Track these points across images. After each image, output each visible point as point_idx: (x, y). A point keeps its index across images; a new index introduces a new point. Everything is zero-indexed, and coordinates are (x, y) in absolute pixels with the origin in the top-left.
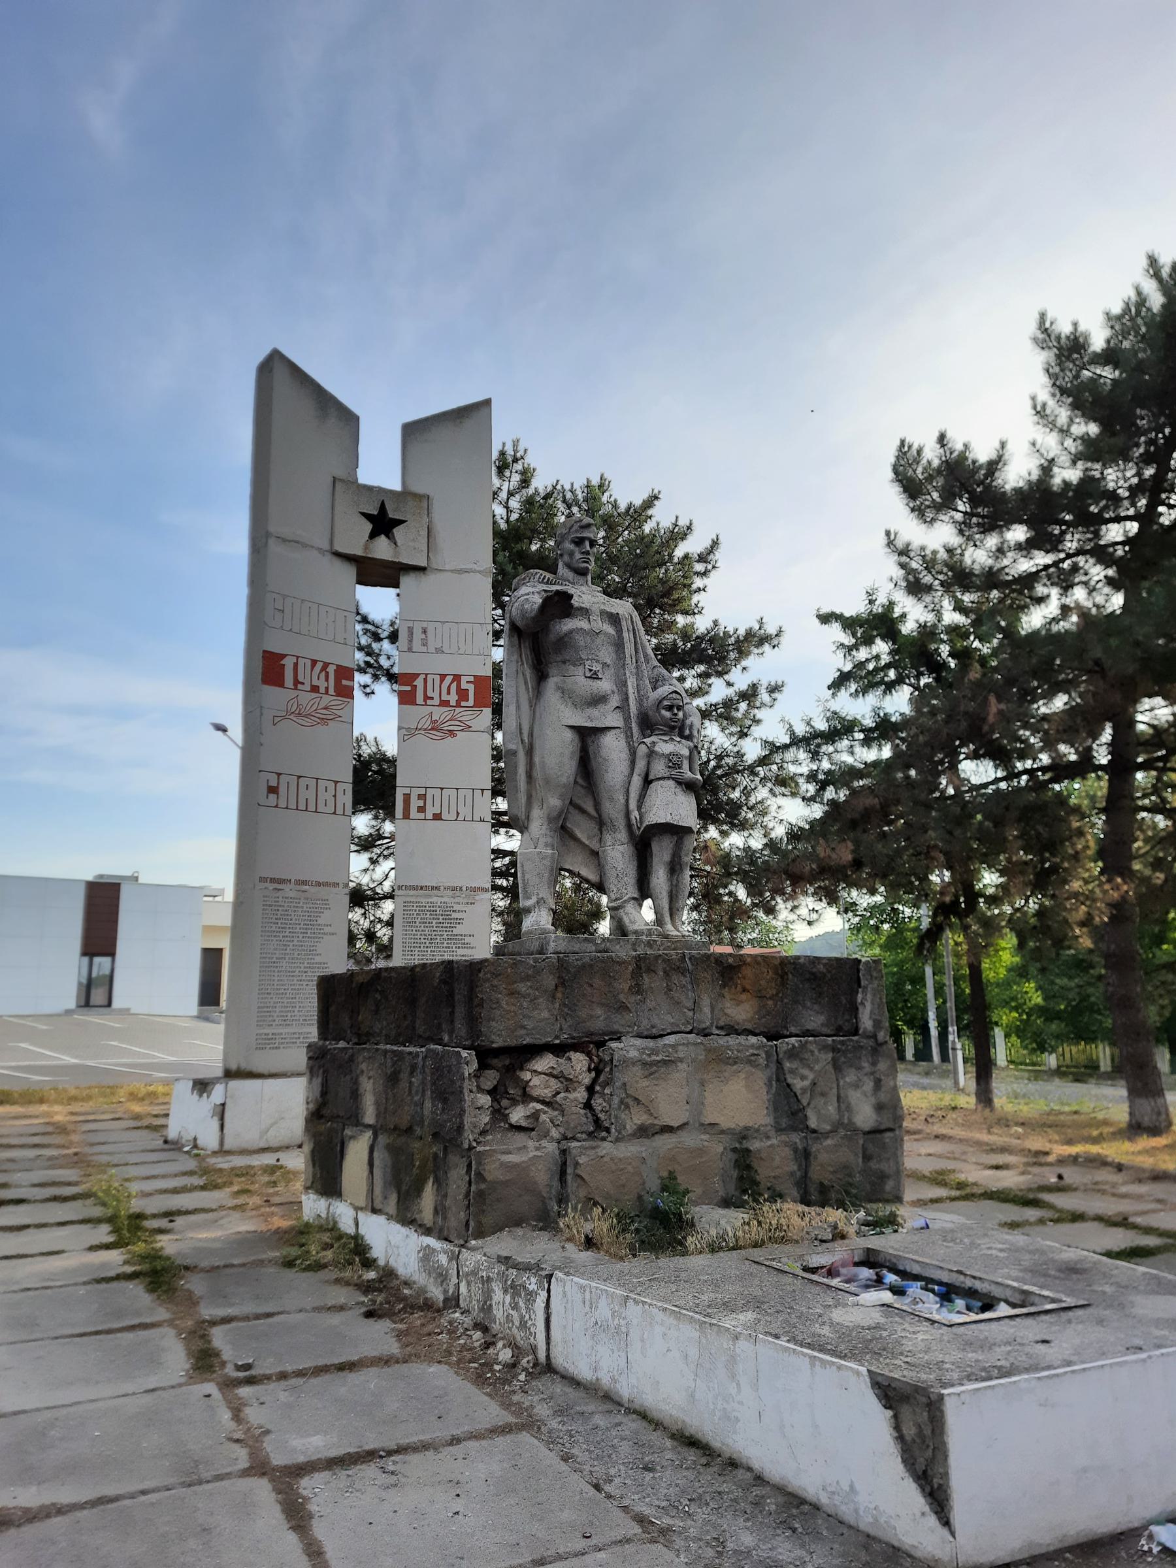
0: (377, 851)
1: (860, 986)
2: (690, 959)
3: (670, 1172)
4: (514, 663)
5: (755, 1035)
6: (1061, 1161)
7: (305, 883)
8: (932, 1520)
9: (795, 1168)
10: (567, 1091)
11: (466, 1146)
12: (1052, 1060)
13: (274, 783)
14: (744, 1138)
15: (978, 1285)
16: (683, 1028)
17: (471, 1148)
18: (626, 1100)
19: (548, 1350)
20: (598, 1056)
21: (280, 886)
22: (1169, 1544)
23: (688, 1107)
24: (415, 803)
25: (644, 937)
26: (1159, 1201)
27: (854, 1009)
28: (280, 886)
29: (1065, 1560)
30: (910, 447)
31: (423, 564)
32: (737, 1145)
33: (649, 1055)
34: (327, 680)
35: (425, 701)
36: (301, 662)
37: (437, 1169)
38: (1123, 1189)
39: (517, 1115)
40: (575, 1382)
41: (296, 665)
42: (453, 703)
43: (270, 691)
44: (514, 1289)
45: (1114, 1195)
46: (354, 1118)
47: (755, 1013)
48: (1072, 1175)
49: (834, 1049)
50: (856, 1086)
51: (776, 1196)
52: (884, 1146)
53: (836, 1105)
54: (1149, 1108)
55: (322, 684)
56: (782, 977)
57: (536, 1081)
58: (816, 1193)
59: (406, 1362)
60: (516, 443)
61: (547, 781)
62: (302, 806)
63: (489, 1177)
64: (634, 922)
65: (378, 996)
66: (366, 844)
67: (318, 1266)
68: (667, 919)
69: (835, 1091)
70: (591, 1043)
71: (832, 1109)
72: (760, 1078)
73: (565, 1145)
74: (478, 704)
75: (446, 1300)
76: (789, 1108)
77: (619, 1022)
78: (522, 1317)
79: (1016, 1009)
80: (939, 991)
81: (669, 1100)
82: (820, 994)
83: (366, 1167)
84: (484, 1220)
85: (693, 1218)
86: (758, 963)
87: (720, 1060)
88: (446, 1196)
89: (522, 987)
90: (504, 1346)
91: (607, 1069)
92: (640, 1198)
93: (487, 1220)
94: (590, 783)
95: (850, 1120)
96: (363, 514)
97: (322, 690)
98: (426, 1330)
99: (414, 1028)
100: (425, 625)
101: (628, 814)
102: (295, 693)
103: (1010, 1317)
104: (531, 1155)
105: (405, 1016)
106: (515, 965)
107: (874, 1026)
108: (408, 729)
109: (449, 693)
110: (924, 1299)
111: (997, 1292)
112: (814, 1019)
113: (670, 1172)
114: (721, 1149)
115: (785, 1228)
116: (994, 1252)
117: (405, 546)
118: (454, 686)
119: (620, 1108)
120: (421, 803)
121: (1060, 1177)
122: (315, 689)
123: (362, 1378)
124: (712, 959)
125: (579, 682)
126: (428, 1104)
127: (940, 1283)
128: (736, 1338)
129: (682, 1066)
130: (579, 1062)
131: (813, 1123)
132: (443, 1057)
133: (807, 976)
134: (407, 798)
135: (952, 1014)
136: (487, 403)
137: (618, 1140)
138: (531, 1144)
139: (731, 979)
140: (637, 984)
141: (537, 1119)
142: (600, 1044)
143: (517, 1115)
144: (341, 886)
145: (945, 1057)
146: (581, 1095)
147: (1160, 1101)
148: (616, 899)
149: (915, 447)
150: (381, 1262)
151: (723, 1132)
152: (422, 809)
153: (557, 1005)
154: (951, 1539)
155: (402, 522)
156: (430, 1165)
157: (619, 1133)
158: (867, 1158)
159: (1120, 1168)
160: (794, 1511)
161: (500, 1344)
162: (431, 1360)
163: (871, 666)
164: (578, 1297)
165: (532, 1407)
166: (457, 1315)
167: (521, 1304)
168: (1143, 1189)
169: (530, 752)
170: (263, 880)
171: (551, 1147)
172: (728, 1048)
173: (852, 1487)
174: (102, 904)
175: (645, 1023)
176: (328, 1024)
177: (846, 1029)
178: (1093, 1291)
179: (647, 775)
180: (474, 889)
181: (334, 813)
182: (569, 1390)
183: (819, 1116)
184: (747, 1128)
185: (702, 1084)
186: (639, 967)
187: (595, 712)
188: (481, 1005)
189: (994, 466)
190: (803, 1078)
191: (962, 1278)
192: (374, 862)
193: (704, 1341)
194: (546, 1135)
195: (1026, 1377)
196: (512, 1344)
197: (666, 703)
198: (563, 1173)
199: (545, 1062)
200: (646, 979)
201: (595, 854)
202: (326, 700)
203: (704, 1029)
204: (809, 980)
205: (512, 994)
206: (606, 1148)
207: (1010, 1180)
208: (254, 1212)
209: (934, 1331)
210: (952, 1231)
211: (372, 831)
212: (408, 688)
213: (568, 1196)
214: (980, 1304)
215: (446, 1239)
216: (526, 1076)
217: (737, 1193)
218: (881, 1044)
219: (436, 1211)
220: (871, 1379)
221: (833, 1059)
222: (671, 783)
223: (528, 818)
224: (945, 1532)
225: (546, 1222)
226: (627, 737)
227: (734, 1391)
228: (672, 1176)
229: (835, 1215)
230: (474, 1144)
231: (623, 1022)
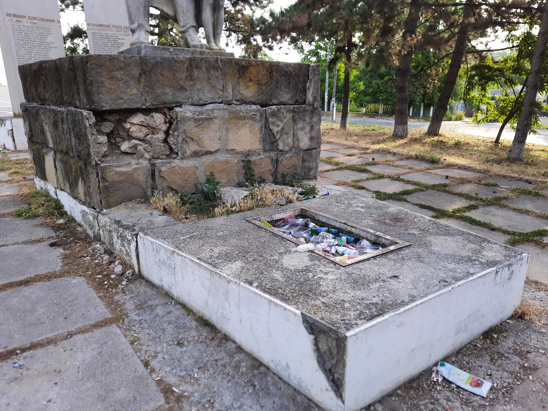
1: (308, 79)
2: (221, 61)
3: (211, 173)
5: (255, 104)
6: (373, 152)
7: (34, 18)
8: (332, 394)
9: (272, 168)
10: (153, 134)
11: (94, 163)
12: (364, 110)
14: (248, 155)
15: (353, 230)
16: (217, 100)
17: (97, 164)
18: (186, 139)
19: (139, 268)
20: (170, 115)
22: (447, 377)
23: (220, 142)
25: (198, 49)
26: (410, 168)
27: (304, 91)
29: (398, 395)
32: (245, 159)
33: (198, 115)
37: (83, 174)
38: (397, 163)
39: (125, 146)
40: (152, 285)
44: (122, 237)
45: (393, 166)
46: (45, 144)
47: (255, 93)
48: (378, 158)
49: (294, 112)
50: (302, 129)
51: (262, 181)
52: (311, 156)
53: (292, 138)
54: (401, 129)
56: (270, 73)
57: (133, 129)
58: (280, 178)
59: (61, 277)
63: (109, 180)
64: (193, 40)
67: (35, 216)
68: (212, 39)
69: (292, 132)
70: (166, 109)
71: (290, 140)
72: (257, 126)
73: (154, 161)
75: (94, 236)
76: (270, 141)
77: (180, 97)
78: (127, 251)
79: (355, 91)
80: (330, 85)
81: (210, 138)
82: (289, 83)
83: (54, 169)
84: (110, 200)
85: (220, 195)
86: (258, 65)
87: (237, 117)
88: (90, 187)
90: (119, 263)
91: (175, 123)
92: (195, 185)
93: (112, 200)
95: (298, 145)
98: (79, 255)
103: (374, 257)
104: (133, 167)
105: (57, 90)
107: (313, 100)
110: (327, 236)
111: (363, 234)
112: (286, 97)
113: (211, 173)
114: (236, 161)
115: (264, 199)
116: (359, 209)
119: (182, 143)
121: (373, 159)
123: (31, 290)
124: (233, 62)
126: (73, 140)
127: (334, 227)
128: (229, 282)
130: (158, 119)
131: (281, 147)
132: (75, 114)
133: (283, 73)
135: (334, 93)
137: (182, 159)
138: (133, 162)
139: (244, 73)
141: (136, 149)
142: (171, 109)
143: (125, 146)
144: (56, 21)
145: (329, 109)
146: (161, 136)
147: (405, 126)
148: (184, 26)
150: (69, 213)
151: (237, 153)
153: (142, 86)
154: (342, 405)
156: (79, 172)
157: (183, 155)
158: (304, 161)
159: (394, 154)
160: (256, 372)
161: (117, 262)
162: (77, 274)
164: (151, 247)
165: (125, 303)
166: (98, 245)
167: (126, 245)
168: (403, 163)
171: (145, 163)
172: (241, 111)
173: (287, 365)
175: (196, 98)
177: (300, 101)
178: (408, 234)
182: (148, 290)
183: (285, 144)
184: (249, 151)
185: (227, 130)
188: (91, 84)
190: (278, 126)
191: (346, 226)
193: (212, 279)
194: (142, 156)
195: (392, 314)
196: (123, 263)
198: (153, 175)
199: (138, 119)
200: (196, 73)
203: (229, 101)
204: (284, 75)
205: (111, 78)
206: (176, 163)
207: (355, 161)
208: (16, 184)
209: (336, 271)
210: (340, 196)
213: (157, 186)
214: (353, 239)
215: (93, 208)
216: (128, 126)
217: (244, 180)
218: (315, 109)
219: (85, 194)
220: (303, 318)
221: (293, 116)
224: (339, 402)
225: (145, 199)
227: (227, 306)
228: (212, 174)
229: (288, 191)
230: (99, 162)
231: (182, 96)
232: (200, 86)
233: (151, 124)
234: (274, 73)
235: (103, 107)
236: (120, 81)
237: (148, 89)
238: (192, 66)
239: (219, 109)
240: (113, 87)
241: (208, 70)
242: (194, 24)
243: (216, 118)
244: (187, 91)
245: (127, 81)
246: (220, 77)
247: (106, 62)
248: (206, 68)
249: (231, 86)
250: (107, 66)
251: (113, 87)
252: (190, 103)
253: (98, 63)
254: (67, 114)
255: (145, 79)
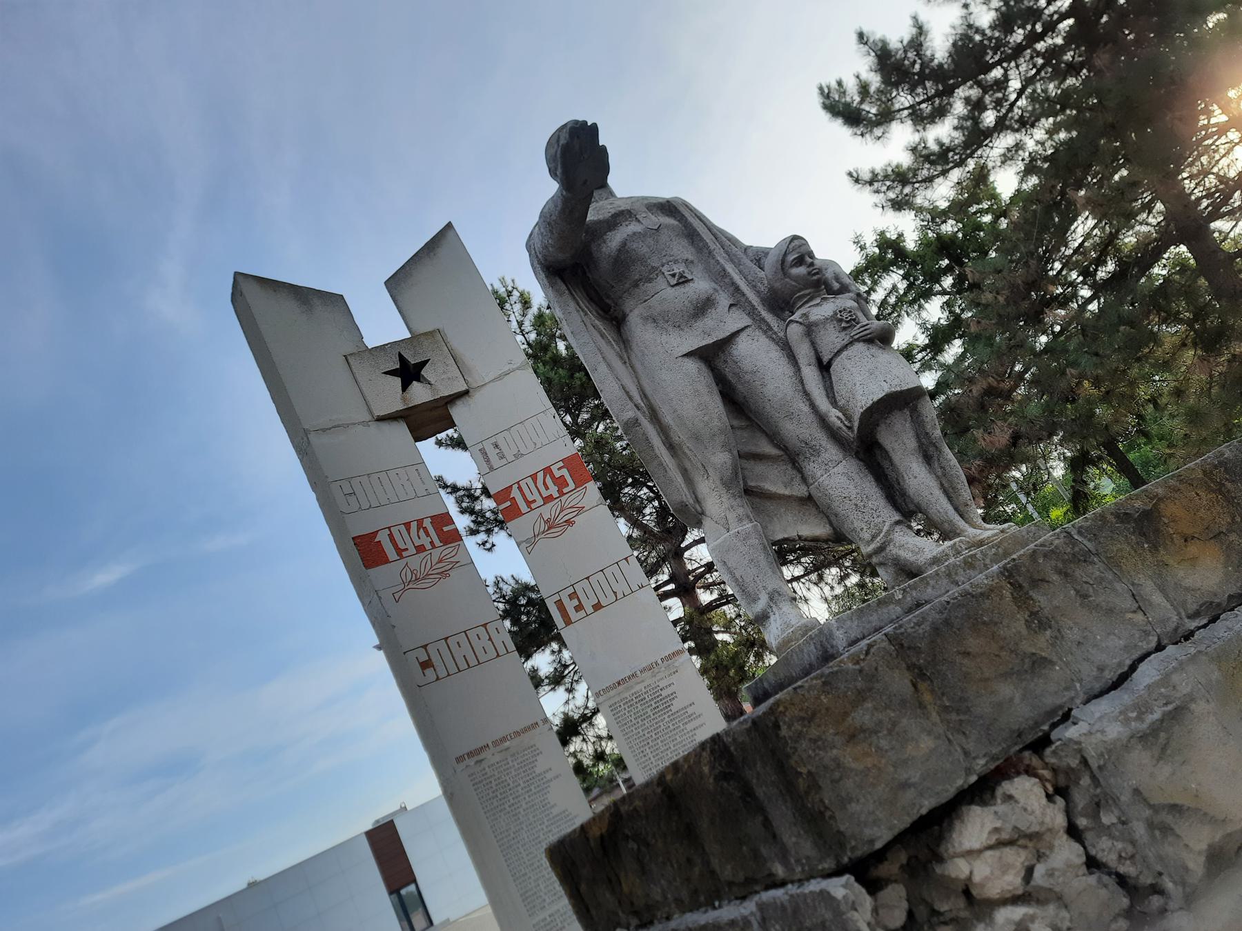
0: (568, 680)
2: (1080, 533)
4: (575, 314)
7: (504, 739)
10: (1040, 856)
13: (424, 658)
21: (480, 757)
24: (570, 605)
25: (952, 560)
28: (480, 757)
30: (829, 87)
31: (463, 388)
33: (1139, 718)
34: (428, 534)
35: (529, 506)
36: (523, 484)
41: (391, 536)
42: (556, 495)
43: (378, 572)
55: (425, 541)
60: (502, 281)
61: (697, 438)
62: (463, 665)
65: (633, 845)
66: (557, 679)
74: (579, 483)
89: (863, 716)
94: (749, 418)
96: (386, 373)
97: (428, 546)
99: (713, 872)
100: (493, 440)
101: (823, 421)
102: (403, 562)
105: (689, 860)
106: (828, 683)
108: (527, 541)
109: (547, 488)
117: (439, 380)
118: (548, 479)
119: (1153, 837)
120: (576, 602)
122: (420, 549)
125: (666, 295)
129: (1199, 707)
130: (1027, 795)
132: (796, 911)
134: (559, 604)
136: (449, 226)
139: (1157, 531)
140: (1032, 614)
144: (540, 723)
148: (874, 537)
149: (834, 85)
152: (579, 608)
153: (935, 717)
155: (424, 363)
157: (1184, 884)
163: (892, 300)
169: (654, 417)
170: (460, 759)
174: (386, 843)
175: (1088, 671)
176: (588, 911)
179: (819, 360)
180: (669, 657)
181: (498, 655)
186: (1017, 587)
187: (708, 322)
188: (815, 786)
189: (916, 44)
192: (570, 691)
197: (791, 258)
199: (975, 828)
200: (1041, 599)
201: (809, 500)
202: (436, 554)
203: (1176, 629)
205: (852, 737)
211: (555, 665)
212: (508, 504)
222: (860, 347)
223: (697, 500)
226: (765, 332)
232: (1076, 630)
233: (1023, 826)
234: (1228, 485)
235: (872, 842)
236: (876, 732)
237: (954, 716)
238: (1020, 586)
239: (1181, 666)
240: (869, 762)
241: (1066, 575)
242: (897, 517)
243: (1191, 698)
244: (1052, 663)
245: (894, 724)
246: (1110, 576)
247: (818, 698)
248: (1059, 572)
249: (1150, 582)
250: (827, 709)
251: (869, 762)
252: (1082, 697)
253: (802, 714)
254: (764, 919)
255: (932, 691)
